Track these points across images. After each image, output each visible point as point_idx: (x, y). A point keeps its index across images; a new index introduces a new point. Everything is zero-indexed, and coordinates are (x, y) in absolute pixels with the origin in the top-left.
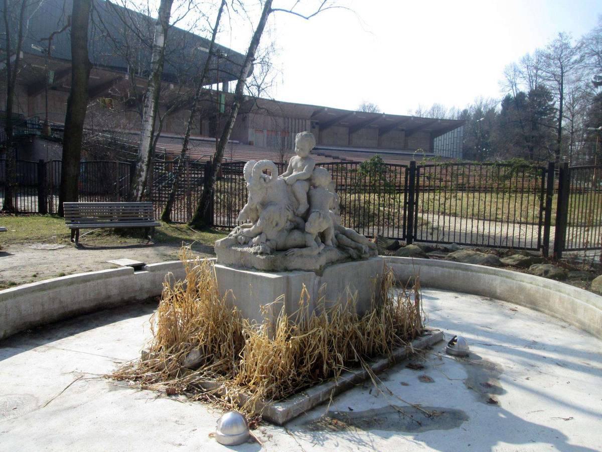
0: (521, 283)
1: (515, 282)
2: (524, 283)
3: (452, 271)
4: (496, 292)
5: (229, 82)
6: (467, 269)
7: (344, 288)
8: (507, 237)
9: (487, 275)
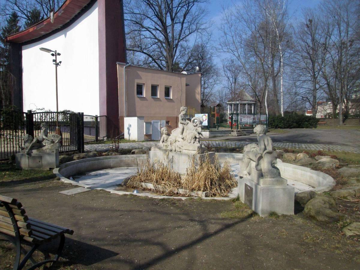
0: (121, 159)
1: (118, 159)
2: (122, 159)
3: (93, 162)
4: (111, 166)
5: (207, 125)
6: (99, 159)
7: (257, 259)
8: (8, 153)
9: (107, 160)
